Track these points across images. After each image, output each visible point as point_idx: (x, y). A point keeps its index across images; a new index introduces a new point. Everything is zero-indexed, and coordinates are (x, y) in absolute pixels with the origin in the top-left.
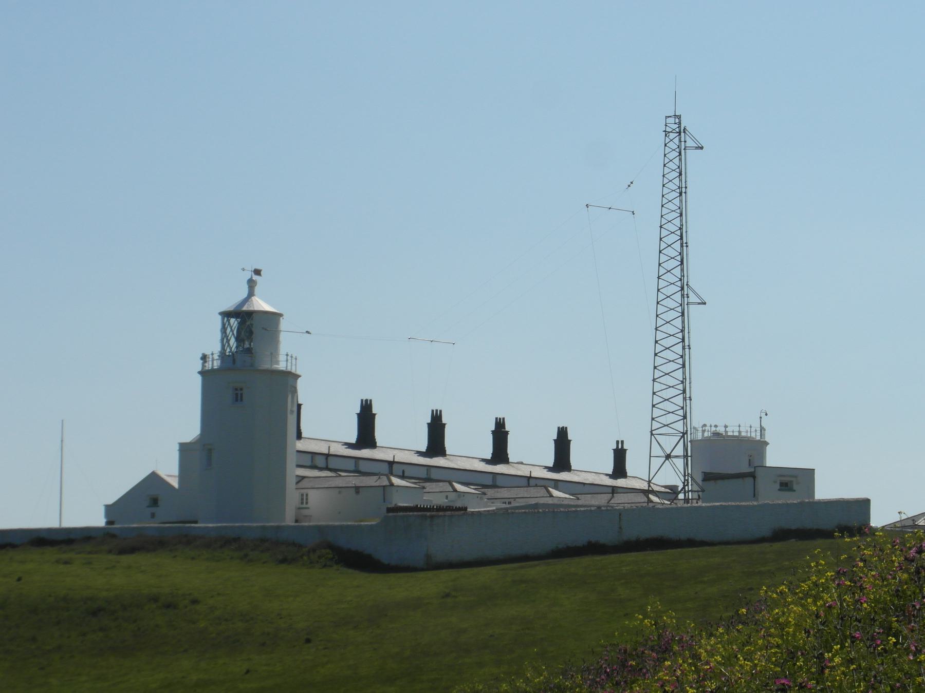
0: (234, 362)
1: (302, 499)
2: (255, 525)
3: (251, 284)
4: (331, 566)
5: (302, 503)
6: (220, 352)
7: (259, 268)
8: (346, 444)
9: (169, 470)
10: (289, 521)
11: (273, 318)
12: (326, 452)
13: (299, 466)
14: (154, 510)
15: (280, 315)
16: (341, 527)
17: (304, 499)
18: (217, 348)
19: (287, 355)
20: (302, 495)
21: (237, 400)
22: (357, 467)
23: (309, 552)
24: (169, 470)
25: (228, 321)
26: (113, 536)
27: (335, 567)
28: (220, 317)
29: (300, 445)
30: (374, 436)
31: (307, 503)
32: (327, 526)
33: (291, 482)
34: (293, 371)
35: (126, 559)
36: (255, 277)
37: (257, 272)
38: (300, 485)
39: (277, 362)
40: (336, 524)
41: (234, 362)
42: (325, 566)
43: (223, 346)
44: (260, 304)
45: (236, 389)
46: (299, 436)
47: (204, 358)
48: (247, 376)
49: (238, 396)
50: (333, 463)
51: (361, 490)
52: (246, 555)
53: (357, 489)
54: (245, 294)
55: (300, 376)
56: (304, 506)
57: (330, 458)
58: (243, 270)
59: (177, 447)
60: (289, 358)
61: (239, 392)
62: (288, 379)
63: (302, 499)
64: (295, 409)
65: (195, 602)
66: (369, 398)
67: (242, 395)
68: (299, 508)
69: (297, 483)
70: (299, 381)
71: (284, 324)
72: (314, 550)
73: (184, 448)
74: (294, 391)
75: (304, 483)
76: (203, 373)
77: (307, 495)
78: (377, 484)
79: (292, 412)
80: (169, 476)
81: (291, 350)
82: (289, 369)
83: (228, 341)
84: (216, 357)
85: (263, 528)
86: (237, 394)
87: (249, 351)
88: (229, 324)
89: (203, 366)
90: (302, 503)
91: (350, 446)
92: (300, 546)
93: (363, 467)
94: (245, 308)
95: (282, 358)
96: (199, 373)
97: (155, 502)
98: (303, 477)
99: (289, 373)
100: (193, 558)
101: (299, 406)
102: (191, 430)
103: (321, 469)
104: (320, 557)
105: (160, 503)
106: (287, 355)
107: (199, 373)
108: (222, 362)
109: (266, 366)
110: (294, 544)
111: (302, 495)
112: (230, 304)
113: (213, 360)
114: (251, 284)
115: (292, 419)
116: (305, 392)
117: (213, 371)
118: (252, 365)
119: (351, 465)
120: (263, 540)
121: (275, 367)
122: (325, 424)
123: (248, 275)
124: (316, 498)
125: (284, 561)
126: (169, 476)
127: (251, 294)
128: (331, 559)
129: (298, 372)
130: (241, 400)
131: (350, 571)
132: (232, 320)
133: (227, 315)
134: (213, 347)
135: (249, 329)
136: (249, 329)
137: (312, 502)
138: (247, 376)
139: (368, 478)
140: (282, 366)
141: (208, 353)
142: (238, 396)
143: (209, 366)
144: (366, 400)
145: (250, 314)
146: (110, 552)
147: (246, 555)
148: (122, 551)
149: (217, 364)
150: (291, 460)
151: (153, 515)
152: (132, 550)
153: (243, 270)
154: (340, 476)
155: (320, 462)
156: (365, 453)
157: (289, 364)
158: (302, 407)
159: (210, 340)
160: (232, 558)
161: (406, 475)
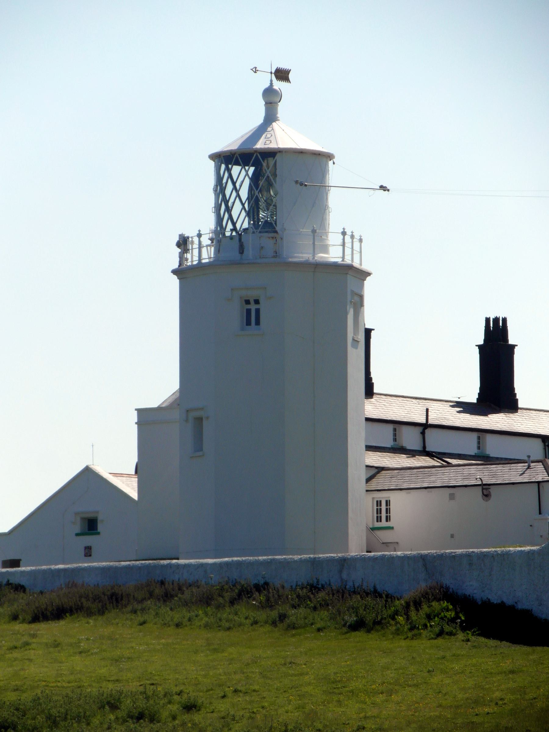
0: (242, 249)
1: (379, 511)
2: (296, 557)
3: (271, 97)
4: (451, 634)
5: (379, 519)
6: (215, 232)
7: (284, 66)
8: (458, 404)
9: (119, 463)
10: (356, 548)
11: (315, 162)
12: (423, 421)
13: (369, 448)
14: (89, 540)
15: (329, 157)
16: (469, 556)
17: (382, 511)
18: (207, 223)
19: (344, 233)
20: (379, 503)
21: (248, 323)
22: (482, 450)
23: (408, 605)
24: (119, 463)
25: (229, 170)
26: (19, 588)
27: (461, 636)
28: (212, 164)
29: (373, 408)
30: (513, 389)
31: (388, 519)
32: (441, 557)
33: (356, 477)
34: (356, 264)
35: (48, 630)
36: (278, 85)
37: (282, 75)
38: (374, 484)
39: (325, 249)
40: (459, 551)
41: (242, 249)
42: (440, 634)
43: (219, 220)
44: (285, 136)
45: (248, 302)
46: (369, 392)
47: (183, 243)
48: (265, 277)
49: (251, 316)
50: (435, 441)
51: (493, 490)
52: (282, 617)
53: (486, 489)
54: (259, 118)
55: (369, 274)
56: (384, 523)
57: (428, 432)
58: (255, 70)
59: (134, 417)
60: (348, 239)
61: (253, 307)
62: (346, 281)
63: (379, 511)
64: (361, 337)
65: (190, 707)
66: (501, 316)
67: (258, 311)
68: (373, 529)
69: (368, 480)
70: (368, 282)
71: (335, 174)
72: (417, 604)
73: (147, 419)
74: (358, 302)
75: (380, 482)
76: (179, 272)
77: (388, 503)
78: (525, 478)
79: (355, 342)
80: (115, 475)
81: (351, 223)
82: (348, 260)
83: (229, 210)
84: (206, 241)
85: (314, 562)
86: (249, 312)
87: (270, 227)
88: (230, 176)
89: (182, 259)
90: (379, 519)
91: (466, 407)
92: (390, 597)
93: (493, 447)
94: (260, 145)
95: (333, 238)
96: (174, 272)
97: (91, 525)
98: (380, 469)
99: (350, 267)
100: (178, 625)
101: (368, 332)
102: (161, 381)
103: (412, 453)
104: (429, 617)
105: (100, 527)
106: (344, 233)
107: (174, 272)
108: (218, 251)
109: (305, 256)
110: (376, 593)
111: (379, 503)
112: (230, 140)
113: (200, 247)
114: (271, 97)
115: (355, 357)
116: (377, 308)
117: (200, 266)
118: (276, 254)
119: (469, 445)
120: (314, 588)
121: (321, 256)
122: (418, 367)
123: (264, 80)
124: (405, 509)
125: (358, 626)
126: (115, 475)
127: (271, 117)
128: (452, 621)
129: (365, 267)
130: (258, 323)
131: (492, 642)
132: (236, 170)
133: (225, 159)
134: (200, 220)
135: (270, 180)
136: (270, 180)
137: (406, 517)
138: (265, 277)
139: (507, 467)
140: (333, 255)
141: (191, 233)
142: (251, 316)
143: (192, 258)
144: (496, 320)
145: (271, 154)
146: (15, 618)
147: (282, 617)
148: (38, 617)
149: (208, 255)
150: (357, 435)
151: (88, 552)
152: (59, 613)
153: (255, 70)
154: (449, 465)
155: (411, 439)
156: (497, 421)
157: (348, 251)
158: (373, 333)
159: (194, 208)
160: (256, 623)
161: (537, 484)
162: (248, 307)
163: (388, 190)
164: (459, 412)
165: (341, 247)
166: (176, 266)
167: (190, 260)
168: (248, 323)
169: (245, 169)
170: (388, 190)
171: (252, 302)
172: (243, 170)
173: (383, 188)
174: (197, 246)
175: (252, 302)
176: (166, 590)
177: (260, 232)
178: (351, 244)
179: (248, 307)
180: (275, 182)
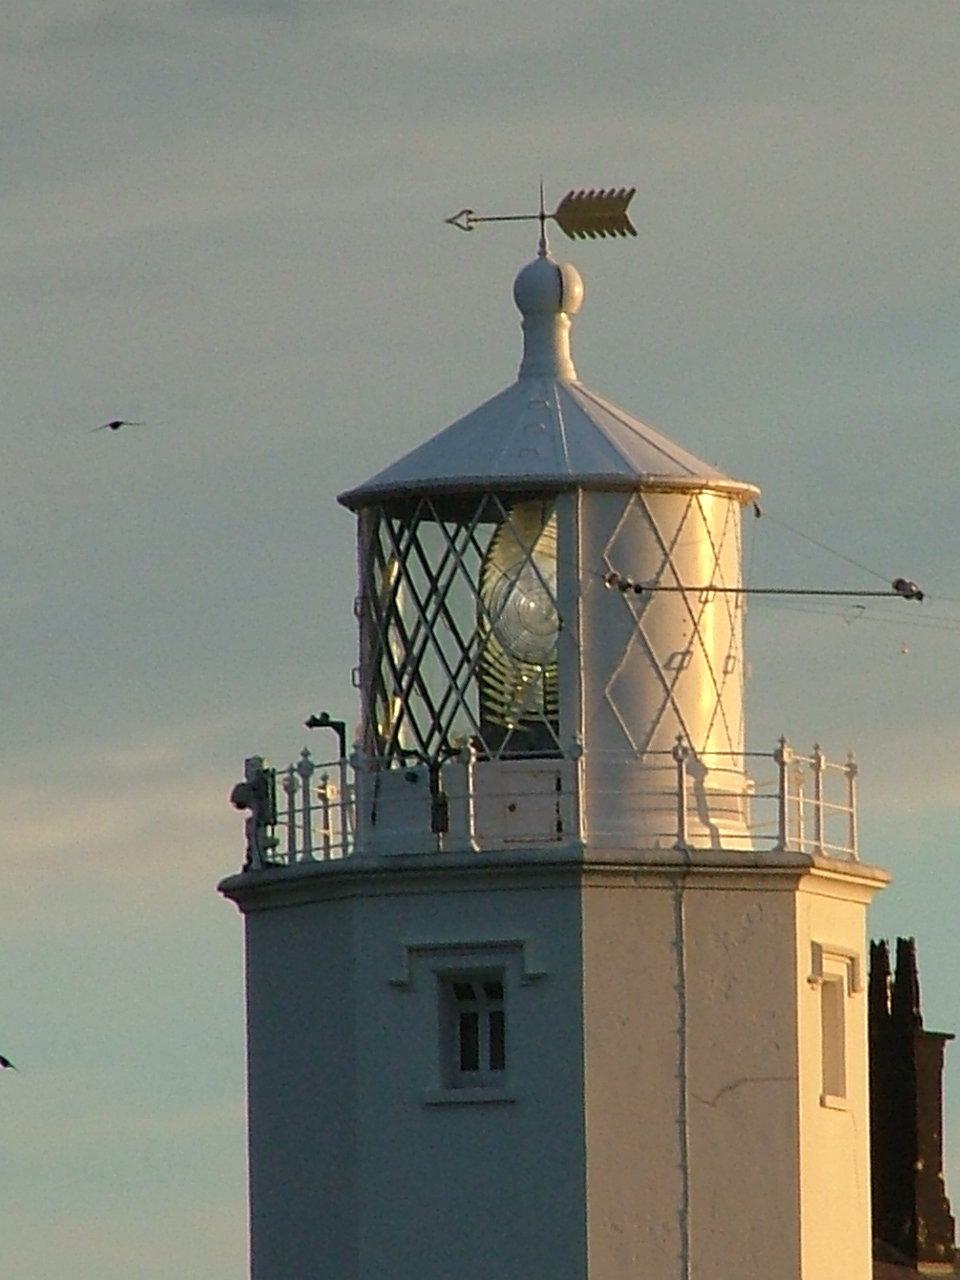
21: (469, 1062)
28: (350, 520)
96: (228, 889)
107: (228, 889)
130: (498, 1061)
162: (469, 1007)
163: (920, 596)
164: (572, 193)
165: (777, 801)
166: (233, 861)
167: (283, 848)
168: (469, 1062)
169: (467, 528)
170: (920, 596)
171: (479, 991)
172: (463, 530)
173: (901, 587)
174: (286, 850)
175: (479, 991)
176: (406, 946)
177: (503, 758)
178: (729, 594)
179: (469, 1007)
180: (557, 733)
